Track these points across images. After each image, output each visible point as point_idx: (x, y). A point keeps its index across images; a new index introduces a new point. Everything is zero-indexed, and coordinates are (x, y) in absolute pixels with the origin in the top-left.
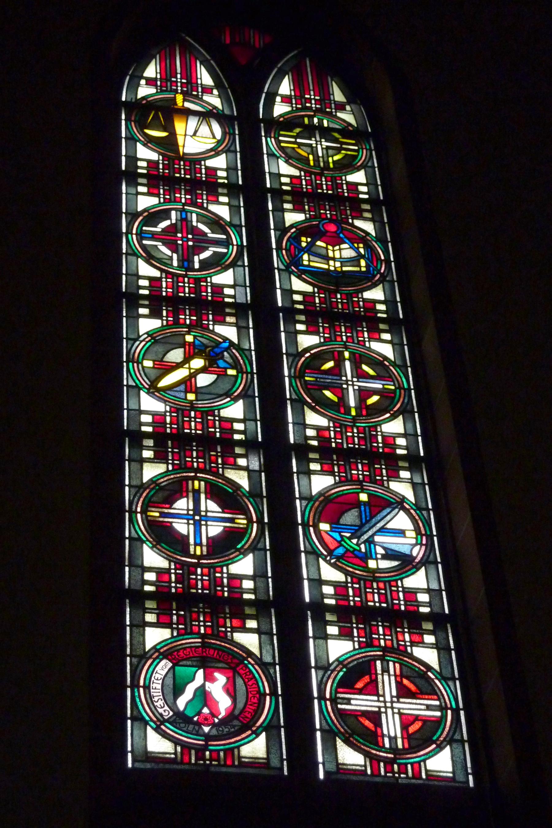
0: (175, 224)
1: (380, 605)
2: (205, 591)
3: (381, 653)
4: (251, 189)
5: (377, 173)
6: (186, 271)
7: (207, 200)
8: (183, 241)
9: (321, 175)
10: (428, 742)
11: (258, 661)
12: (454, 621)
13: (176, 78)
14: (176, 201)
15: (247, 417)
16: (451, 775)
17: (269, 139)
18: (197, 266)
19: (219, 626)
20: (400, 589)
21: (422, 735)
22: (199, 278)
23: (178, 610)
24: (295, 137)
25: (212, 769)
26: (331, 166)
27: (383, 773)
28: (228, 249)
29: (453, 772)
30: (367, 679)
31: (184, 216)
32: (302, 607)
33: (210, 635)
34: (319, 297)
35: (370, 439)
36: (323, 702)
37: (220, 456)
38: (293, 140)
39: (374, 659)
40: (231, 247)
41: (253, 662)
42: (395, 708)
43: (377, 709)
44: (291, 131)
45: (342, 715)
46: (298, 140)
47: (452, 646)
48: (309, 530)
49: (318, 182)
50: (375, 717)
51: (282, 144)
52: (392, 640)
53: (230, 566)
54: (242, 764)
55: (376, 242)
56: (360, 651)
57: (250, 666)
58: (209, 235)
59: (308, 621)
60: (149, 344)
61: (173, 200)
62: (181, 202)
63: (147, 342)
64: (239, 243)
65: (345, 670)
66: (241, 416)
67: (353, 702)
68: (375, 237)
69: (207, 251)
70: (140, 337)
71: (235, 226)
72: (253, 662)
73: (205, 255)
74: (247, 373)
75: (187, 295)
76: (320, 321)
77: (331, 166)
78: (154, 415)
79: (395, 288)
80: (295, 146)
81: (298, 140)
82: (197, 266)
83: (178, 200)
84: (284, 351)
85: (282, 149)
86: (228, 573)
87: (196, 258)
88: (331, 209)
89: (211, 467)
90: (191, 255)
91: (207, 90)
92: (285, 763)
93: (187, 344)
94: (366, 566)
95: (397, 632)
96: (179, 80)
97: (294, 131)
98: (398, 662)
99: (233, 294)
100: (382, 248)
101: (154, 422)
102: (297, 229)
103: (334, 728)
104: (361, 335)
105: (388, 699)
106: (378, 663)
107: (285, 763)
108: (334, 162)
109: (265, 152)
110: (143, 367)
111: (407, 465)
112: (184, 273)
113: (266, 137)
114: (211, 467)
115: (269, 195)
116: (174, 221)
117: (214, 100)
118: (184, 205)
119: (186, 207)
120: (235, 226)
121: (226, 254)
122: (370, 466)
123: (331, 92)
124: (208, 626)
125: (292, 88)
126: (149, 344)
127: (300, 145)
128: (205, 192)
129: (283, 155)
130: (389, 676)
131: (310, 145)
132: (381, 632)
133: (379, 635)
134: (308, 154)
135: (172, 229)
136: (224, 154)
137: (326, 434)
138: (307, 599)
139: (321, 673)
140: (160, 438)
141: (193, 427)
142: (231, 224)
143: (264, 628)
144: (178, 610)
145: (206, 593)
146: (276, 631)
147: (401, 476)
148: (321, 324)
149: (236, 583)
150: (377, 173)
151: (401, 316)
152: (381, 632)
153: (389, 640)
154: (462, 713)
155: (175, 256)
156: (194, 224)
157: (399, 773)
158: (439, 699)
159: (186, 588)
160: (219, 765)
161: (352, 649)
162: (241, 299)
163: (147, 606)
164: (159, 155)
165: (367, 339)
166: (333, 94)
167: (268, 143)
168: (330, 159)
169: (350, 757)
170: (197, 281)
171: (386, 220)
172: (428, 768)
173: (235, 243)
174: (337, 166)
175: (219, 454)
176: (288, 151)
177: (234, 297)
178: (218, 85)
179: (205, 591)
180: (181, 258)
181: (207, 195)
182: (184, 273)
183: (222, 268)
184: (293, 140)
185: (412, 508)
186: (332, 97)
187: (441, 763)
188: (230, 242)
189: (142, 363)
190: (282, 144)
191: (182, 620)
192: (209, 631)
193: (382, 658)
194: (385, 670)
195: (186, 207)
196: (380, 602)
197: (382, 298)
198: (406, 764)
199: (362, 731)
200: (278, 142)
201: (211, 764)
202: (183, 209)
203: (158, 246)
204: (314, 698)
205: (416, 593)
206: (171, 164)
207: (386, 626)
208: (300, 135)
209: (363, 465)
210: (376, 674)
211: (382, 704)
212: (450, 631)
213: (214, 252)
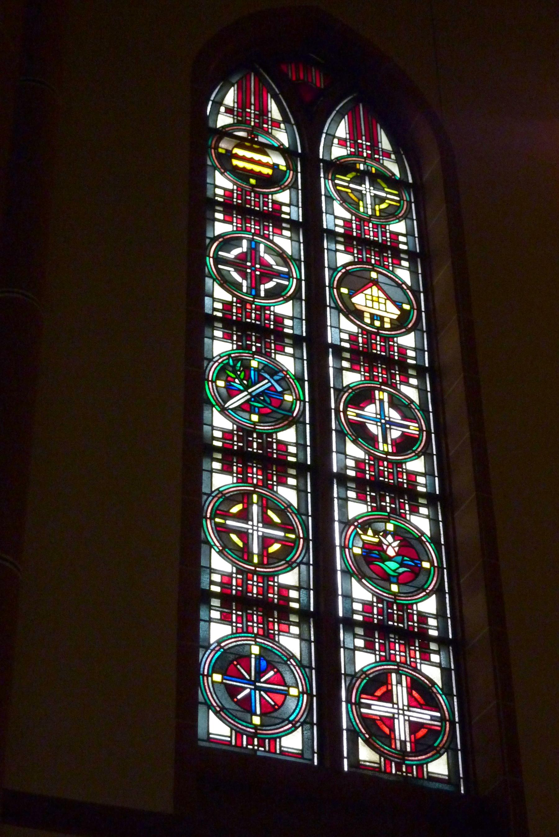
0: (246, 253)
1: (407, 774)
2: (259, 596)
3: (396, 667)
4: (311, 230)
5: (456, 703)
6: (254, 298)
7: (273, 232)
8: (251, 270)
9: (369, 221)
10: (431, 748)
11: (298, 662)
12: (433, 373)
13: (250, 109)
14: (247, 230)
15: (295, 316)
16: (447, 778)
17: (327, 181)
18: (262, 294)
19: (268, 480)
20: (415, 612)
21: (425, 741)
22: (265, 306)
23: (237, 463)
24: (349, 182)
25: (259, 753)
26: (378, 214)
27: (394, 772)
28: (289, 281)
29: (449, 776)
30: (383, 689)
31: (253, 246)
32: (337, 620)
33: (260, 486)
34: (377, 606)
35: (389, 349)
36: (349, 705)
37: (275, 474)
38: (346, 184)
39: (390, 671)
40: (291, 279)
41: (294, 664)
42: (406, 715)
43: (391, 715)
44: (345, 176)
45: (364, 718)
46: (352, 186)
47: (429, 389)
48: (345, 551)
49: (389, 611)
50: (390, 721)
51: (338, 188)
52: (406, 657)
53: (278, 434)
54: (282, 753)
55: (429, 543)
56: (364, 382)
57: (289, 514)
58: (274, 267)
59: (334, 484)
60: (221, 500)
61: (244, 229)
62: (250, 232)
63: (219, 498)
64: (298, 277)
65: (367, 678)
66: (288, 202)
67: (373, 707)
68: (419, 406)
69: (271, 282)
70: (214, 358)
71: (295, 260)
72: (294, 664)
73: (270, 285)
74: (300, 401)
75: (255, 451)
76: (368, 490)
77: (378, 214)
78: (223, 575)
79: (438, 514)
80: (349, 191)
81: (352, 186)
82: (262, 294)
83: (249, 229)
84: (332, 385)
85: (338, 192)
86: (272, 199)
87: (262, 287)
88: (374, 249)
89: (266, 352)
90: (258, 284)
91: (276, 124)
92: (316, 755)
93: (252, 368)
94: (390, 590)
95: (410, 650)
96: (252, 120)
97: (348, 176)
98: (409, 676)
99: (288, 211)
100: (437, 554)
101: (224, 195)
102: (353, 391)
103: (350, 569)
104: (386, 260)
105: (401, 717)
106: (394, 676)
107: (316, 755)
108: (380, 210)
109: (323, 193)
110: (217, 386)
111: (406, 257)
112: (252, 299)
113: (325, 178)
114: (264, 234)
115: (330, 350)
116: (245, 250)
117: (282, 137)
118: (253, 235)
119: (255, 237)
120: (295, 260)
121: (287, 286)
122: (387, 370)
123: (380, 140)
124: (260, 586)
125: (348, 132)
126: (221, 500)
127: (353, 190)
128: (271, 225)
129: (339, 199)
130: (402, 687)
131: (360, 191)
132: (397, 649)
133: (396, 651)
134: (359, 200)
135: (242, 257)
136: (288, 191)
137: (362, 466)
138: (341, 614)
139: (331, 272)
140: (226, 599)
141: (253, 318)
142: (292, 258)
143: (297, 355)
144: (237, 463)
145: (260, 598)
146: (314, 637)
147: (420, 512)
148: (368, 493)
149: (284, 592)
150: (456, 703)
151: (451, 637)
152: (397, 649)
153: (403, 656)
154: (413, 205)
155: (245, 283)
156: (262, 254)
157: (407, 772)
158: (417, 423)
159: (245, 580)
160: (265, 751)
161: (374, 661)
162: (294, 217)
163: (212, 604)
164: (234, 185)
165: (408, 512)
166: (381, 142)
167: (325, 185)
168: (377, 207)
169: (366, 754)
170: (260, 308)
171: (440, 519)
172: (429, 770)
173: (295, 276)
174: (383, 214)
175: (274, 473)
176: (343, 194)
177: (289, 214)
178: (286, 120)
179: (259, 596)
180: (249, 286)
181: (273, 227)
182: (252, 299)
183: (281, 189)
184: (346, 184)
185: (416, 408)
186: (380, 144)
187: (439, 767)
188: (291, 275)
189: (215, 382)
190: (338, 188)
191: (240, 619)
192: (261, 632)
193: (397, 672)
194: (399, 682)
195: (255, 237)
196: (381, 351)
197: (422, 470)
198: (412, 766)
199: (378, 731)
200: (335, 185)
201: (258, 750)
202: (253, 239)
203: (231, 272)
204: (339, 595)
205: (406, 349)
206: (245, 580)
207: (402, 644)
208: (353, 180)
209: (382, 369)
210: (392, 685)
211: (396, 711)
212: (439, 507)
213: (278, 283)
